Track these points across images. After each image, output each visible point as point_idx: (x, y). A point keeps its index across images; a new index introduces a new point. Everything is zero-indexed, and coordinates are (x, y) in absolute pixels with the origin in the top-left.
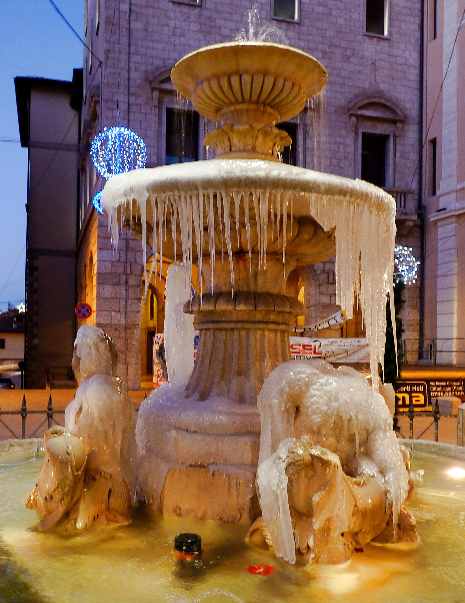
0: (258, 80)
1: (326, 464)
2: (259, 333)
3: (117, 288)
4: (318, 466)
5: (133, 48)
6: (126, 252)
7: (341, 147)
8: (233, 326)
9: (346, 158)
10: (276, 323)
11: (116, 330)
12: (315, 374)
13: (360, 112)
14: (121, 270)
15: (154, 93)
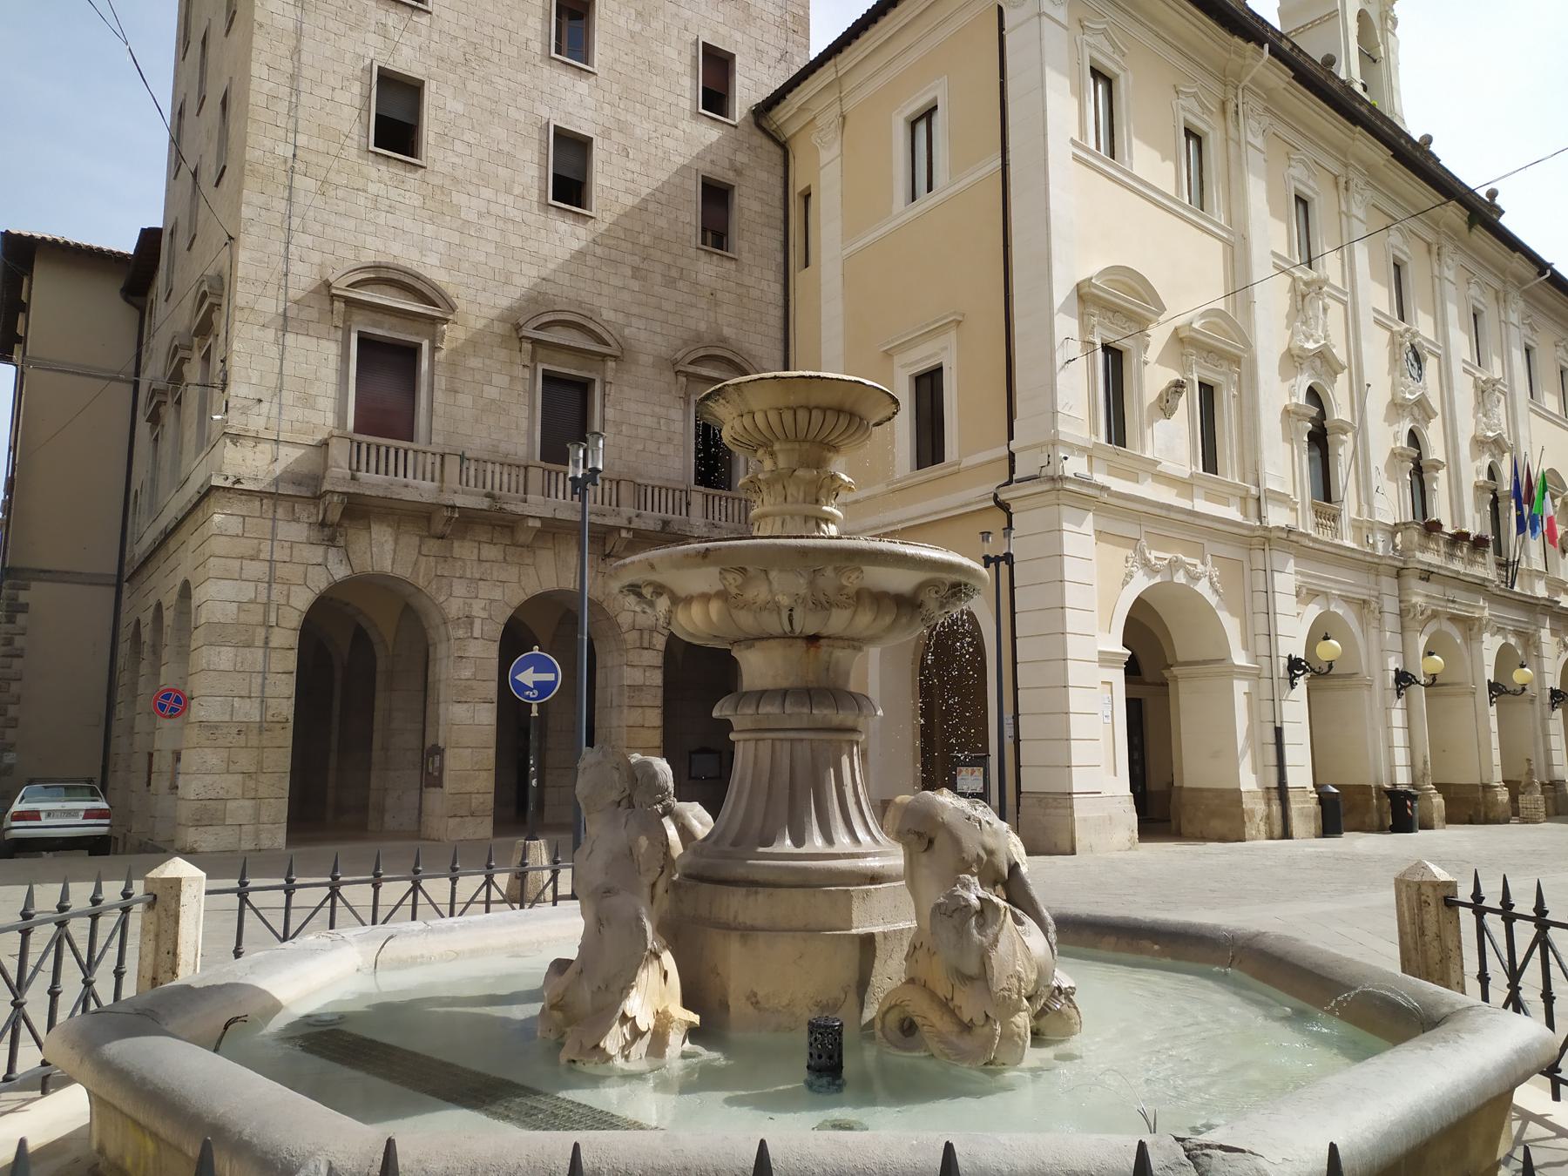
5: (296, 222)
9: (670, 440)
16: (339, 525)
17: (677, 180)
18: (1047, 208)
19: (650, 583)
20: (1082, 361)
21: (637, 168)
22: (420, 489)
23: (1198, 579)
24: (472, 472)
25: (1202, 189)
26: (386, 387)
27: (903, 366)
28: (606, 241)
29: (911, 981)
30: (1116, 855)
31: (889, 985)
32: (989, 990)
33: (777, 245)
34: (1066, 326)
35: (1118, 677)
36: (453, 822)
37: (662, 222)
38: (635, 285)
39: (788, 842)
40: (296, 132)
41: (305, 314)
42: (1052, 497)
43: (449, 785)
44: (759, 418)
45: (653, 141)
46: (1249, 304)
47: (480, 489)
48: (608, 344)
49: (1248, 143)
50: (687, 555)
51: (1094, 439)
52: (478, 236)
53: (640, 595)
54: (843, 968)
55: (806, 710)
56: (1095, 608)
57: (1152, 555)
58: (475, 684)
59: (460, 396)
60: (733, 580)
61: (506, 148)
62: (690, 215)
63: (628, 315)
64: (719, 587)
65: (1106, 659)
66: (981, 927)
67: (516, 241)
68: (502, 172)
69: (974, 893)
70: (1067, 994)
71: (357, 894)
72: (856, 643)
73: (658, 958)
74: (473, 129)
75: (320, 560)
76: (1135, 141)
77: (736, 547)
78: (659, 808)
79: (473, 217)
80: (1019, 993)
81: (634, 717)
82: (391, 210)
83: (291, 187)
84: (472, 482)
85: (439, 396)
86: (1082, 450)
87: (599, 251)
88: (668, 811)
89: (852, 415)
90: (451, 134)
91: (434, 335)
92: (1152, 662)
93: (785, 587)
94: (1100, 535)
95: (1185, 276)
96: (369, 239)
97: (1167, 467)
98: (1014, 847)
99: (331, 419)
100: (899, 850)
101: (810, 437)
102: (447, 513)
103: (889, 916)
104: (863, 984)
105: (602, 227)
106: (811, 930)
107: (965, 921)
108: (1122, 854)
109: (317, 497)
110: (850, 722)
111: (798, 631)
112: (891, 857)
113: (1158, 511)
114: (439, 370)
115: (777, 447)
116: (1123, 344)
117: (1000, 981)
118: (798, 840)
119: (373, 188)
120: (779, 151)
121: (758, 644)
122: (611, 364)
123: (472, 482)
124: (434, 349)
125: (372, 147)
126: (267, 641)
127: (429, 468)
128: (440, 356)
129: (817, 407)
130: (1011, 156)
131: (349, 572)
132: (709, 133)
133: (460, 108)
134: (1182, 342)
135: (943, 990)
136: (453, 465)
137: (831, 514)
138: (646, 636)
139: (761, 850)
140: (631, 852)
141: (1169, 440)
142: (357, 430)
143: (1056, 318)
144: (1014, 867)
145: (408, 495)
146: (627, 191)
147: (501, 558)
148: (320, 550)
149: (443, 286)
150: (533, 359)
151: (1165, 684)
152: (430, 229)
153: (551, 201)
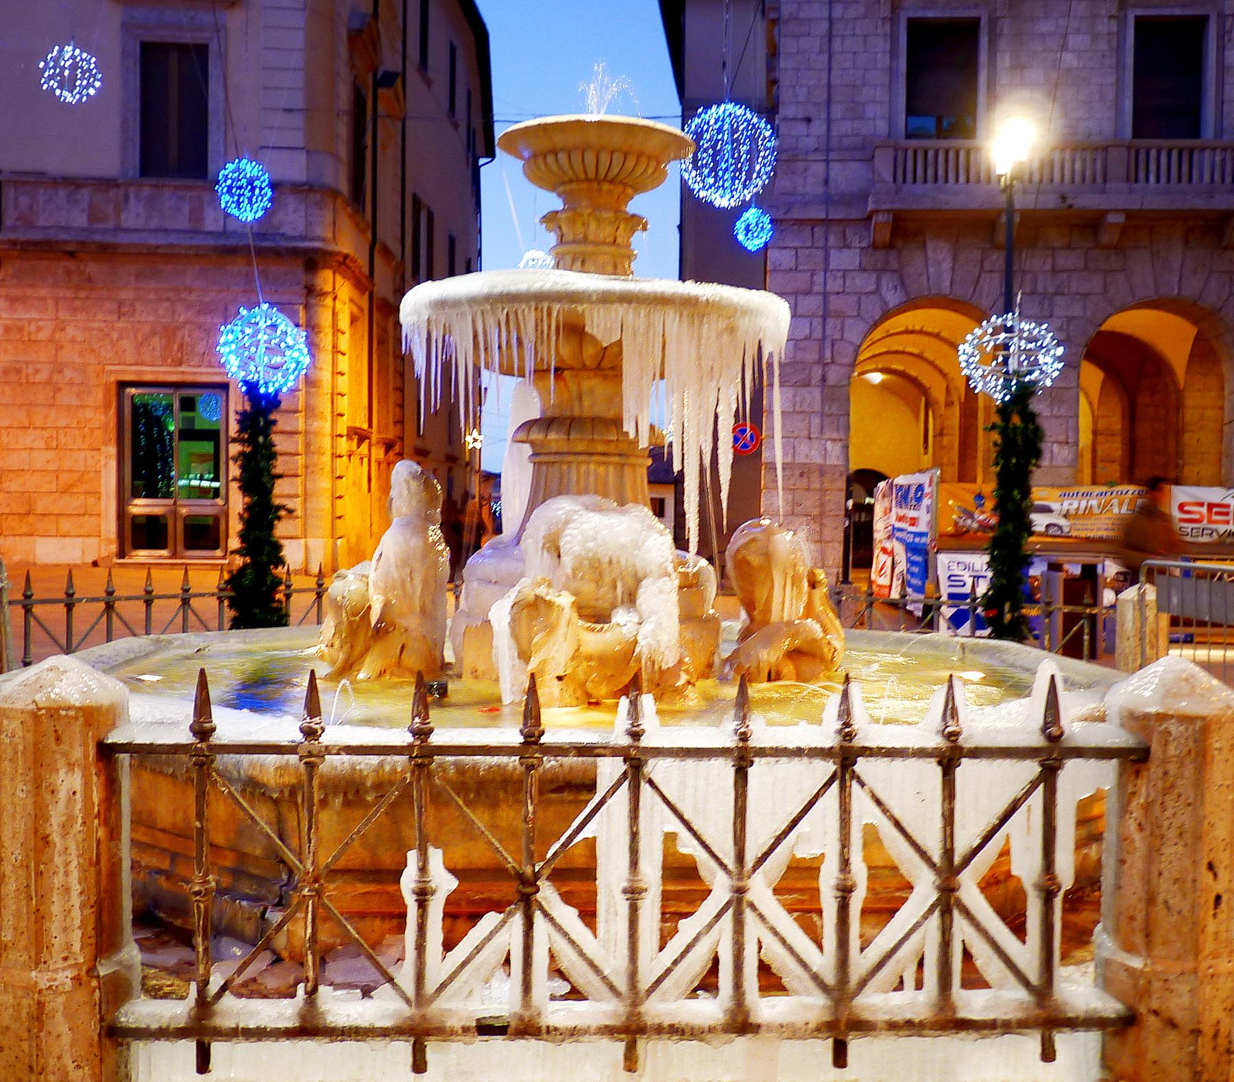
0: (590, 158)
1: (549, 605)
2: (583, 468)
3: (805, 390)
4: (542, 605)
6: (825, 320)
8: (551, 458)
10: (604, 454)
11: (801, 475)
12: (576, 512)
14: (813, 356)
50: (114, 873)
99: (882, 126)
101: (611, 176)
126: (824, 379)
147: (1081, 265)
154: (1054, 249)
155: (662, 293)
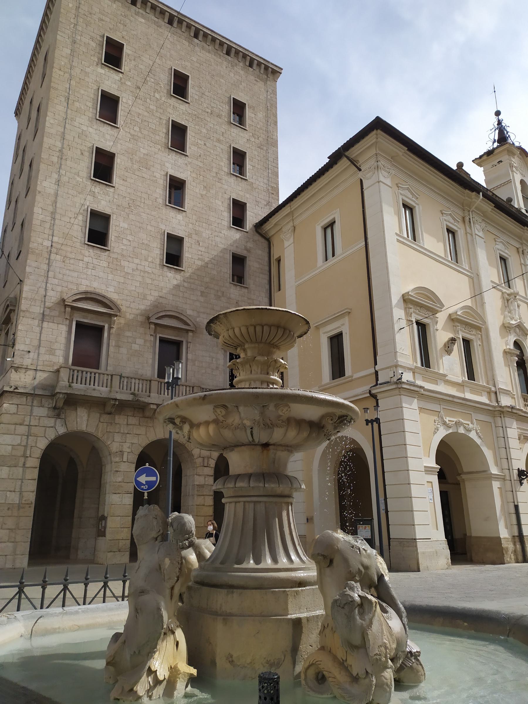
5: (51, 274)
7: (214, 360)
9: (217, 368)
13: (75, 305)
15: (67, 309)
16: (62, 408)
17: (221, 255)
18: (387, 262)
19: (179, 417)
20: (407, 329)
21: (203, 250)
22: (101, 391)
23: (470, 431)
24: (125, 383)
25: (456, 254)
26: (88, 346)
27: (324, 333)
28: (189, 280)
29: (322, 648)
30: (440, 572)
31: (310, 650)
32: (367, 654)
33: (266, 281)
34: (398, 313)
35: (435, 479)
36: (109, 555)
37: (215, 272)
38: (202, 299)
39: (252, 562)
40: (53, 236)
41: (53, 313)
42: (397, 391)
43: (108, 536)
44: (237, 331)
45: (210, 237)
46: (483, 304)
47: (129, 391)
48: (188, 325)
49: (476, 234)
50: (195, 399)
51: (415, 364)
52: (131, 278)
53: (174, 424)
54: (284, 641)
55: (261, 485)
56: (419, 420)
57: (447, 419)
58: (122, 484)
59: (121, 349)
60: (221, 412)
61: (146, 242)
62: (227, 269)
63: (198, 312)
64: (213, 417)
65: (428, 470)
66: (362, 614)
67: (149, 281)
68: (143, 252)
69: (357, 593)
70: (415, 656)
71: (77, 589)
72: (290, 448)
73: (173, 633)
74: (131, 234)
75: (52, 425)
76: (424, 234)
77: (220, 393)
78: (187, 542)
79: (130, 271)
80: (386, 657)
81: (199, 500)
82: (94, 269)
83: (49, 259)
84: (125, 388)
85: (111, 349)
86: (410, 369)
87: (186, 284)
88: (192, 545)
89: (285, 329)
90: (122, 236)
91: (110, 322)
92: (452, 469)
93: (247, 415)
94: (421, 409)
95: (453, 292)
96: (83, 280)
97: (450, 377)
98: (381, 565)
99: (61, 360)
100: (313, 565)
102: (112, 402)
103: (309, 608)
104: (295, 650)
105: (187, 275)
106: (264, 616)
107: (352, 611)
108: (444, 571)
109: (53, 395)
110: (286, 492)
111: (257, 441)
112: (310, 572)
113: (448, 398)
114: (112, 337)
115: (247, 346)
116: (425, 321)
117: (374, 650)
118: (258, 561)
119: (86, 259)
120: (266, 242)
121: (236, 449)
122: (190, 334)
123: (125, 388)
124: (110, 328)
125: (86, 242)
127: (105, 381)
128: (113, 331)
129: (266, 325)
130: (369, 241)
131: (65, 431)
132: (236, 235)
133: (126, 226)
134: (453, 319)
135: (340, 654)
136: (116, 379)
137: (275, 380)
138: (206, 461)
139: (236, 566)
140: (160, 568)
141: (451, 365)
142: (73, 364)
143: (394, 310)
144: (381, 577)
145: (95, 394)
146: (199, 259)
147: (137, 423)
148: (52, 420)
149: (115, 300)
150: (155, 332)
151: (458, 484)
152: (110, 277)
153: (165, 264)
154: (128, 416)
155: (427, 606)
